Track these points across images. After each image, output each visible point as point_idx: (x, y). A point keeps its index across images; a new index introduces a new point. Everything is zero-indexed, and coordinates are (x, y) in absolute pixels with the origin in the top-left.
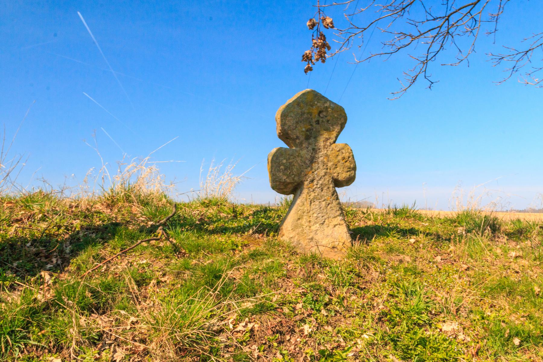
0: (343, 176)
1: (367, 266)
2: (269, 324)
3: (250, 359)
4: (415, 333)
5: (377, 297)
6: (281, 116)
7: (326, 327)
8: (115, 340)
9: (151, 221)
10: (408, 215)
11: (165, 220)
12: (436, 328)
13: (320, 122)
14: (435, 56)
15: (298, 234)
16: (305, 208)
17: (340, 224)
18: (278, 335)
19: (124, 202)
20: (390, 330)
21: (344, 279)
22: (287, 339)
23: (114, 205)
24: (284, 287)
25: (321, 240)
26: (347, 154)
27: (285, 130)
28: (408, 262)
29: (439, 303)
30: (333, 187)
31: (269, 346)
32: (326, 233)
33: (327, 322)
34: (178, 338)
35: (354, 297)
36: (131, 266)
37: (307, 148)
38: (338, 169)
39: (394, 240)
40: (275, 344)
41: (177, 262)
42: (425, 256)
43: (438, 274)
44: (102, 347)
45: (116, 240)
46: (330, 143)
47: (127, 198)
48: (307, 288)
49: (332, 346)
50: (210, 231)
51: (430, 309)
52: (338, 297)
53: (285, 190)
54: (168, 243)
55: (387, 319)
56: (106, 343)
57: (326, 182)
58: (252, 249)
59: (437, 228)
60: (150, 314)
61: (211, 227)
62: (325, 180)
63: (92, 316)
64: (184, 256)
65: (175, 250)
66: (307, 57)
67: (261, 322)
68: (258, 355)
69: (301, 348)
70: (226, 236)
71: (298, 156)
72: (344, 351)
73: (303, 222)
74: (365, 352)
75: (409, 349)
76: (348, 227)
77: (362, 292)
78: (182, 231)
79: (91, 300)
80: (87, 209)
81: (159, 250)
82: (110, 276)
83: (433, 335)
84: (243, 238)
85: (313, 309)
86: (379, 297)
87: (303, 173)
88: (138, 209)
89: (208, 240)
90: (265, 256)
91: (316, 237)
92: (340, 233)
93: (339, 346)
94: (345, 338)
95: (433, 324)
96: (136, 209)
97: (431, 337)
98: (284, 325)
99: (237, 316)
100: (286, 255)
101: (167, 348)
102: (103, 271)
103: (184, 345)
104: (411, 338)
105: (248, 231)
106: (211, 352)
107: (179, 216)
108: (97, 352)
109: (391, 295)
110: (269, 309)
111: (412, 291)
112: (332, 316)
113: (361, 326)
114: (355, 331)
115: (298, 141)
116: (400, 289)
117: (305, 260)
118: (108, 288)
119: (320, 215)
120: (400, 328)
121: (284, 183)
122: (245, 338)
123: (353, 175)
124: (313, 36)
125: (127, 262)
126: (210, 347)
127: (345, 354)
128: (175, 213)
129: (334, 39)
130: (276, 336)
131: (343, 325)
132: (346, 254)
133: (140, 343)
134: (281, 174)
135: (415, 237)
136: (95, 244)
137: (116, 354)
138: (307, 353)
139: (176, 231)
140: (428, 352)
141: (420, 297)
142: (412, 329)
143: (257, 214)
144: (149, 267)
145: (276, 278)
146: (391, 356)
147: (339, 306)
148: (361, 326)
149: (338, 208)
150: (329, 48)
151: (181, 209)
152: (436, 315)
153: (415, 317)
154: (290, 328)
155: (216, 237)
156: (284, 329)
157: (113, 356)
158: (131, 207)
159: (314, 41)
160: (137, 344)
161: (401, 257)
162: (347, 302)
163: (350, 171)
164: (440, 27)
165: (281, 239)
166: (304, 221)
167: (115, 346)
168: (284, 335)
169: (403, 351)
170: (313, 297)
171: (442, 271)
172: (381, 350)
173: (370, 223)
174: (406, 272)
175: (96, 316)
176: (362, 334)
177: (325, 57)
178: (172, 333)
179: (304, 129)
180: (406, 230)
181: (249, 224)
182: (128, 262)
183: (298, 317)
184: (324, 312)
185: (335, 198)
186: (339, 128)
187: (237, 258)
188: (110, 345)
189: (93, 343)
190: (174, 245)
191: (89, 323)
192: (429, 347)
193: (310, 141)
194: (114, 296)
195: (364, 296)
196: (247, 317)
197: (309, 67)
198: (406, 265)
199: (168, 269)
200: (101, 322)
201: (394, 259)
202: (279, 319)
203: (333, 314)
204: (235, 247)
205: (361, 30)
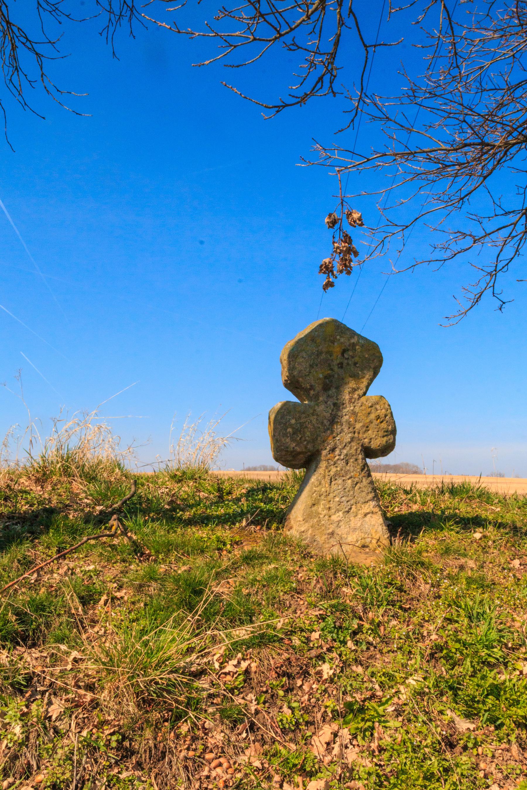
0: (377, 443)
1: (412, 575)
2: (272, 662)
3: (245, 715)
4: (484, 678)
5: (428, 621)
6: (289, 357)
7: (354, 668)
8: (50, 685)
9: (99, 505)
10: (470, 494)
11: (119, 503)
12: (515, 669)
13: (345, 364)
14: (507, 264)
15: (312, 527)
16: (323, 489)
17: (372, 513)
18: (284, 679)
19: (61, 476)
20: (447, 672)
21: (379, 595)
22: (298, 685)
23: (46, 480)
24: (293, 607)
25: (345, 536)
26: (383, 411)
27: (294, 376)
28: (472, 569)
29: (518, 632)
30: (363, 459)
31: (272, 696)
32: (352, 524)
33: (356, 660)
34: (141, 685)
35: (394, 622)
36: (72, 574)
37: (326, 403)
38: (370, 432)
39: (451, 535)
40: (281, 693)
41: (139, 568)
42: (497, 560)
43: (515, 587)
44: (31, 696)
45: (51, 534)
46: (359, 395)
47: (66, 471)
48: (327, 609)
49: (363, 696)
50: (185, 520)
51: (505, 641)
52: (372, 622)
53: (294, 463)
54: (126, 540)
55: (442, 655)
56: (36, 690)
57: (353, 451)
58: (246, 548)
59: (513, 516)
60: (100, 646)
61: (187, 515)
62: (351, 448)
63: (17, 650)
64: (148, 559)
65: (135, 551)
66: (327, 267)
67: (260, 660)
68: (256, 710)
69: (318, 700)
70: (208, 528)
71: (313, 414)
72: (381, 704)
73: (320, 509)
74: (411, 705)
75: (475, 701)
76: (384, 515)
77: (406, 614)
78: (146, 522)
79: (16, 627)
80: (8, 486)
81: (112, 549)
82: (43, 590)
83: (510, 680)
84: (233, 532)
85: (335, 640)
86: (431, 622)
87: (319, 439)
88: (81, 487)
89: (183, 535)
90: (265, 560)
91: (338, 531)
92: (375, 526)
93: (373, 696)
94: (382, 685)
95: (510, 664)
96: (78, 486)
97: (507, 683)
98: (293, 664)
99: (225, 650)
100: (295, 559)
101: (125, 699)
102: (33, 581)
103: (150, 695)
104: (478, 685)
105: (240, 521)
106: (188, 705)
107: (140, 497)
108: (24, 703)
109: (449, 619)
110: (272, 640)
111: (478, 613)
112: (362, 651)
113: (405, 666)
114: (396, 674)
115: (312, 392)
116: (461, 610)
117: (323, 566)
118: (40, 608)
119: (343, 499)
120: (461, 670)
121: (292, 452)
122: (237, 683)
123: (391, 441)
124: (334, 237)
125: (66, 567)
126: (187, 697)
127: (382, 708)
128: (135, 493)
129: (362, 241)
130: (281, 681)
131: (379, 665)
132: (382, 558)
133: (86, 690)
134: (288, 440)
135: (481, 530)
136: (21, 541)
137: (52, 707)
138: (326, 707)
139: (136, 521)
140: (503, 706)
141: (490, 622)
142: (480, 671)
143: (253, 494)
144: (98, 575)
145: (282, 594)
146: (448, 712)
147: (372, 636)
148: (405, 666)
149: (370, 490)
150: (356, 254)
151: (143, 485)
152: (513, 649)
153: (484, 653)
154: (301, 668)
155: (194, 530)
156: (295, 670)
157: (47, 710)
158: (70, 483)
159: (336, 245)
160: (82, 692)
161: (463, 561)
162: (385, 630)
163: (387, 435)
164: (515, 224)
165: (288, 533)
166: (320, 508)
167: (50, 694)
168: (294, 678)
169: (467, 704)
170: (335, 623)
171: (521, 582)
172: (434, 702)
173: (415, 508)
174: (468, 583)
175: (23, 650)
176: (407, 678)
177: (351, 267)
178: (133, 677)
179: (321, 376)
180: (468, 519)
181: (242, 510)
182: (69, 569)
183: (314, 653)
184: (350, 644)
185: (366, 474)
186: (371, 373)
187: (225, 563)
188: (43, 693)
189: (18, 690)
190: (133, 542)
191: (12, 660)
192: (504, 697)
193: (330, 392)
194: (49, 619)
195: (409, 621)
196: (240, 652)
197: (329, 281)
198: (470, 573)
199: (125, 580)
200: (31, 659)
201: (452, 564)
202: (286, 656)
203: (364, 647)
204: (221, 546)
205: (401, 228)
